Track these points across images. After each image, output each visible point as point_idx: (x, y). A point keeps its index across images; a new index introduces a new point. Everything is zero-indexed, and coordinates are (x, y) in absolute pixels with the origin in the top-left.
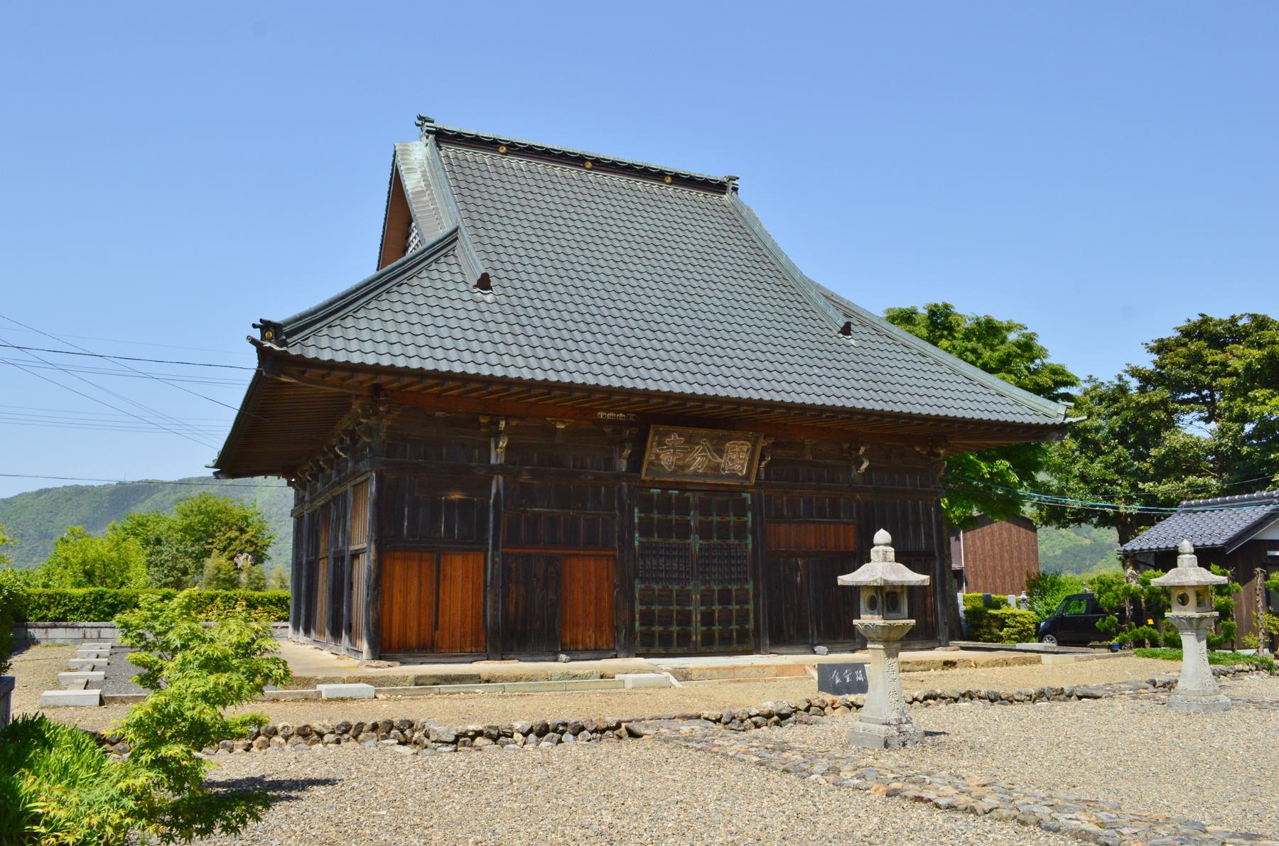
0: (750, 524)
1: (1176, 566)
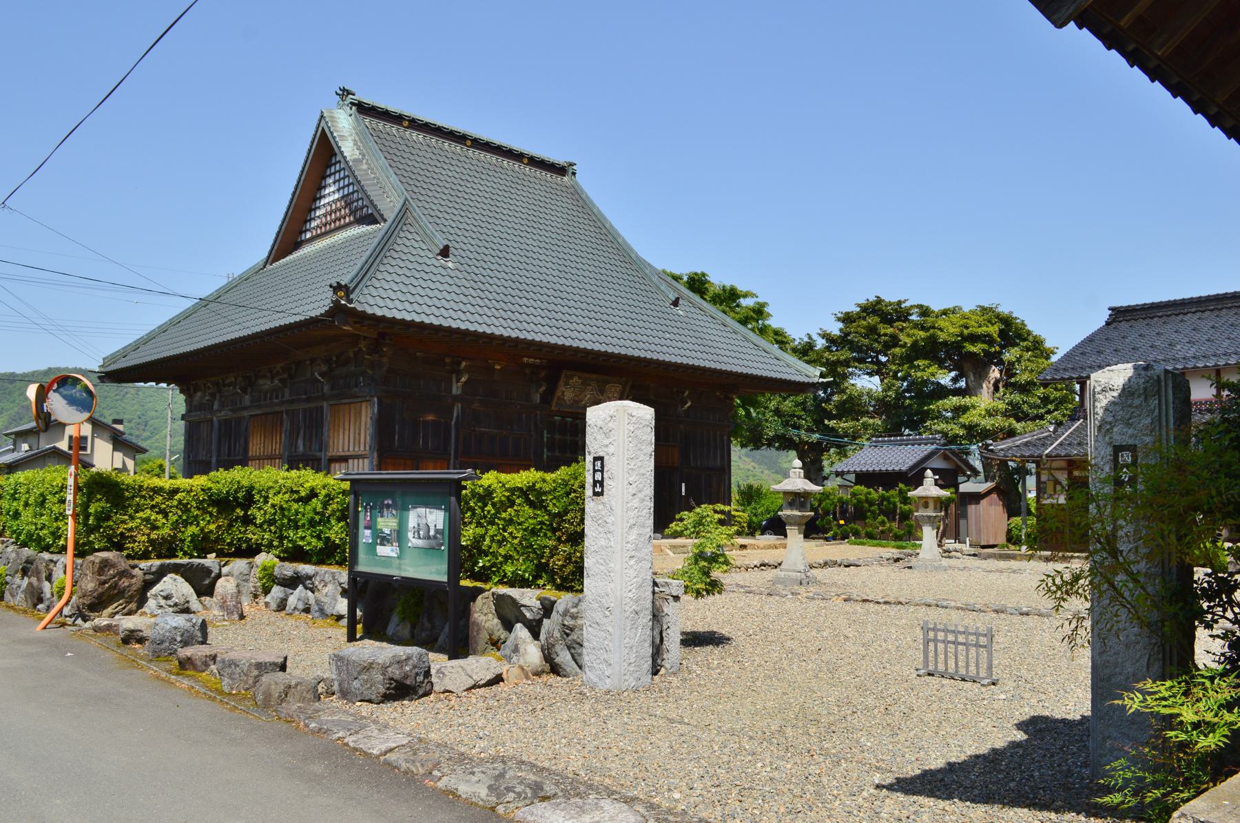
1: (922, 485)
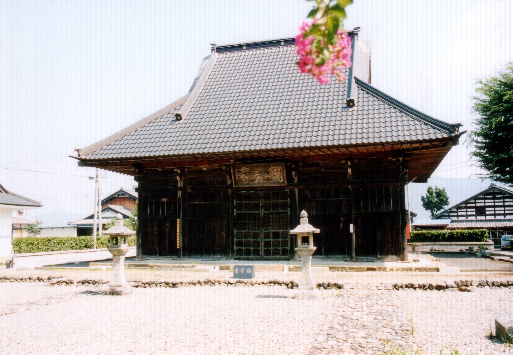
0: (289, 203)
